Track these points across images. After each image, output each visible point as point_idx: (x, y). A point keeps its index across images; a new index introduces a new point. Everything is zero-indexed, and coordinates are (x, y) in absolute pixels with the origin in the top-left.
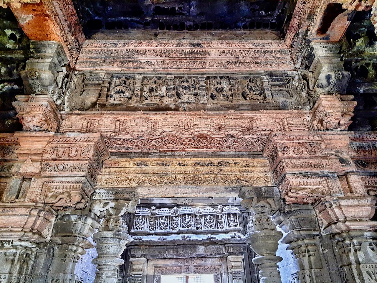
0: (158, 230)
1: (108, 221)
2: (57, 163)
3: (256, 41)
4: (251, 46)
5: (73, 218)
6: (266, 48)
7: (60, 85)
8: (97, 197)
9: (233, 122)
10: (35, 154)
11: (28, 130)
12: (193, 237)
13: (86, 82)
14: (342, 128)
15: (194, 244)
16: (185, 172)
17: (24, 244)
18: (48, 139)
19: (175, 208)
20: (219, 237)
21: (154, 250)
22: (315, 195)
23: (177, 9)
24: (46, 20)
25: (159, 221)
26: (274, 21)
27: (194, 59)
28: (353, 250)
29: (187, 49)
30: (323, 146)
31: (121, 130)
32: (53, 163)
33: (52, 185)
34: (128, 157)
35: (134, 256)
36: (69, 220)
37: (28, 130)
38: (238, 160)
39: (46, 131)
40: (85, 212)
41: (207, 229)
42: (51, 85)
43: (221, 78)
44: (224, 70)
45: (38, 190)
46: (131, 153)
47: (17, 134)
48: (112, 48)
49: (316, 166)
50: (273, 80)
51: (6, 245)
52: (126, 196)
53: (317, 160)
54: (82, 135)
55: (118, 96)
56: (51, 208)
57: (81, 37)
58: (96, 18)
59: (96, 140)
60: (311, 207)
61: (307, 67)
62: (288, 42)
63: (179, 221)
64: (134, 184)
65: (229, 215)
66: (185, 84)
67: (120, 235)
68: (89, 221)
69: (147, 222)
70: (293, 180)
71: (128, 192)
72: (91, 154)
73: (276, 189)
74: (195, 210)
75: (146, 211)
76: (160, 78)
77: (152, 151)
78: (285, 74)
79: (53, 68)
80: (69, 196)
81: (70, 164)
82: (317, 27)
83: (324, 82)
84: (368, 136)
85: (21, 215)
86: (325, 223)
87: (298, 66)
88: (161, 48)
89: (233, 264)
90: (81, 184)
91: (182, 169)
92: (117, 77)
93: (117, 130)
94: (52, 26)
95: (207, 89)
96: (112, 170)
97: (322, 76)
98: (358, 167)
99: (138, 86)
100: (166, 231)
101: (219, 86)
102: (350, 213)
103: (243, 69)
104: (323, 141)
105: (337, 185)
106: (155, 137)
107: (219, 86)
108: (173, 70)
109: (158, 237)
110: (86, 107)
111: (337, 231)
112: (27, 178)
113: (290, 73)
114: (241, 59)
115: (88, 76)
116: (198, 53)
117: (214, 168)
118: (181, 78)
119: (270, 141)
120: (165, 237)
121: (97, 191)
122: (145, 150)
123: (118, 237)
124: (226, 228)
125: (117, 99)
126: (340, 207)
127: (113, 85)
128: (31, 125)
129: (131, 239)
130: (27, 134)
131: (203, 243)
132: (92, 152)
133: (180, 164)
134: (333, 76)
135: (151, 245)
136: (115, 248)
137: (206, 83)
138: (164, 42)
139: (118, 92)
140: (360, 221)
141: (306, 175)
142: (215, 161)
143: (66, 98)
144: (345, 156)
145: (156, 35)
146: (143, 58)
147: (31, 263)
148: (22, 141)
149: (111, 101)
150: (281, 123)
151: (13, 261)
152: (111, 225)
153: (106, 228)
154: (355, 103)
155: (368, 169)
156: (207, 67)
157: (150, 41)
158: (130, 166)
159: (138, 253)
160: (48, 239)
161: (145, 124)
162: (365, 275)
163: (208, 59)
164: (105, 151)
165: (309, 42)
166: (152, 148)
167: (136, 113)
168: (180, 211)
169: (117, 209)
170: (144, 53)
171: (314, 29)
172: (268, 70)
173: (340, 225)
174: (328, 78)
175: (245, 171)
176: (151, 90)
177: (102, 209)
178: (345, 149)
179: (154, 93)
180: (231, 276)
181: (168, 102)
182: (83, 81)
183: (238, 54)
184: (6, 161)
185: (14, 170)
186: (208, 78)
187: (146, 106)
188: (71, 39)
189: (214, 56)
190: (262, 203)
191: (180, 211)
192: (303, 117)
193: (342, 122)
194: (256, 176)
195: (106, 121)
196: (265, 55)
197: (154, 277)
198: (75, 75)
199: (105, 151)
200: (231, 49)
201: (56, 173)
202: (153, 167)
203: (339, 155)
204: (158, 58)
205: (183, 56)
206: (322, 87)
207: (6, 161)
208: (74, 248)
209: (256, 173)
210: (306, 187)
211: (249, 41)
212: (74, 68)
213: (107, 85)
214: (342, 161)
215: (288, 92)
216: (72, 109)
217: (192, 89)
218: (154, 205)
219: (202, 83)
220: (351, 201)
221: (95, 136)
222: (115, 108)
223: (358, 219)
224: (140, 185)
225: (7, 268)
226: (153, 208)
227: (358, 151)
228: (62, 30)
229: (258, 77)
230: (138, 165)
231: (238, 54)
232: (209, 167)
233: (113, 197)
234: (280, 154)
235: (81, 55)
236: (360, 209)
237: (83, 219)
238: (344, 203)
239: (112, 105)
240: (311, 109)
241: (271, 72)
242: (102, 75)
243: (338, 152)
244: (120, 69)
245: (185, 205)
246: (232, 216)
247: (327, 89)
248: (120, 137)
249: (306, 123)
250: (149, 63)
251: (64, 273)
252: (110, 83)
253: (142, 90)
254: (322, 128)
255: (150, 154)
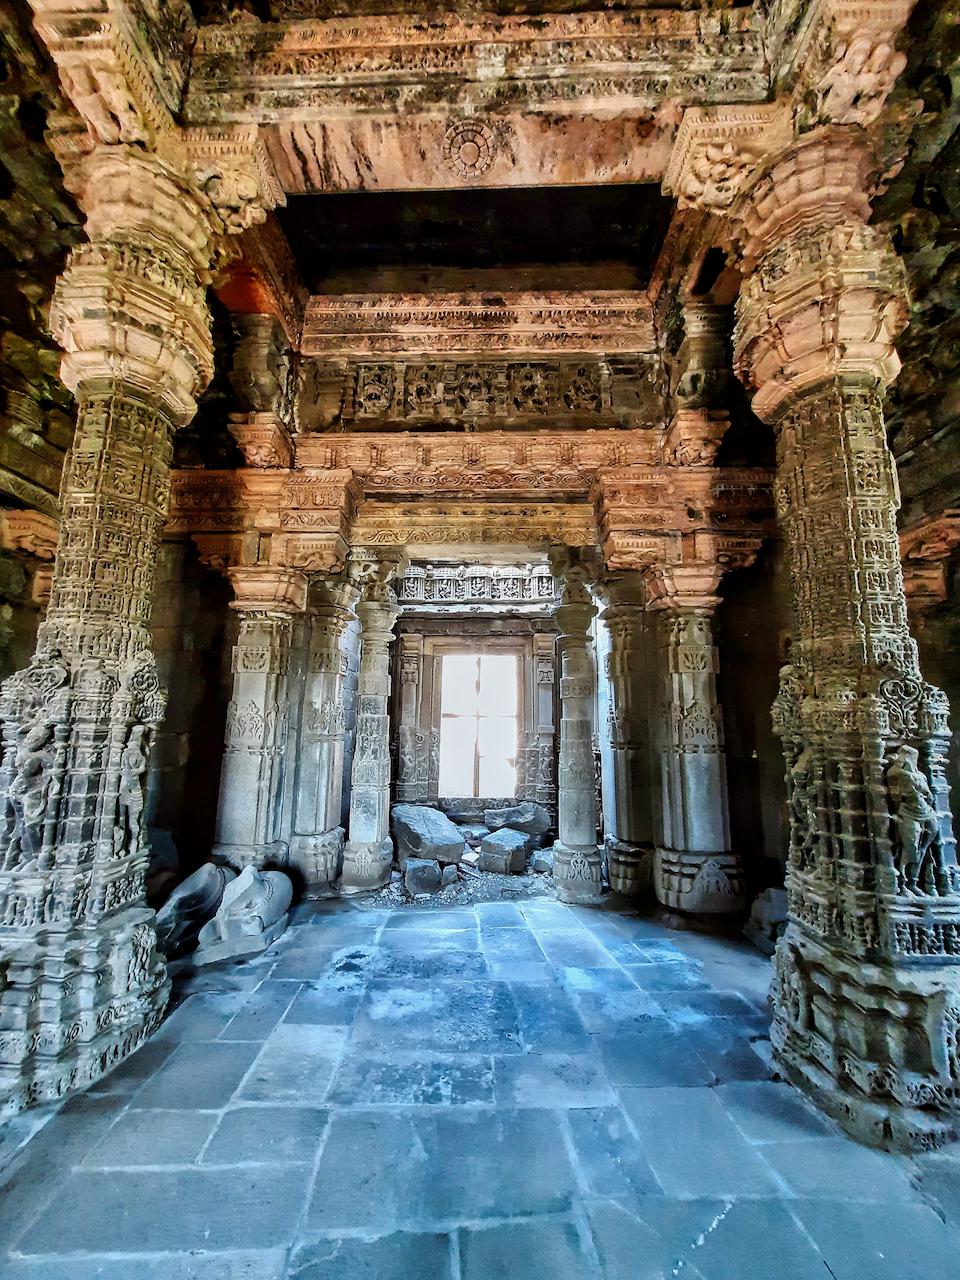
0: (437, 599)
1: (371, 588)
2: (300, 513)
3: (598, 293)
4: (588, 301)
5: (329, 584)
6: (615, 306)
7: (285, 391)
8: (353, 558)
9: (543, 449)
10: (269, 502)
11: (253, 466)
12: (487, 609)
13: (320, 380)
14: (704, 462)
15: (488, 619)
16: (472, 524)
17: (278, 615)
18: (282, 479)
19: (462, 567)
20: (524, 609)
21: (431, 625)
22: (645, 561)
23: (461, 223)
24: (252, 281)
25: (438, 586)
26: (636, 245)
27: (489, 331)
28: (676, 629)
29: (479, 309)
30: (671, 491)
31: (380, 463)
32: (294, 514)
33: (299, 544)
34: (389, 501)
35: (405, 631)
36: (324, 586)
37: (253, 466)
38: (549, 506)
39: (279, 467)
40: (342, 577)
41: (507, 598)
42: (273, 395)
43: (532, 365)
44: (538, 351)
45: (283, 550)
46: (395, 494)
47: (240, 472)
48: (354, 310)
49: (654, 520)
50: (617, 371)
51: (259, 616)
52: (393, 557)
53: (657, 512)
54: (327, 473)
55: (370, 404)
56: (303, 574)
57: (302, 292)
58: (323, 246)
59: (346, 480)
60: (639, 576)
61: (674, 351)
62: (653, 294)
63: (467, 586)
64: (402, 541)
65: (540, 578)
66: (474, 381)
67: (388, 606)
68: (348, 588)
69: (421, 586)
70: (618, 540)
71: (394, 552)
72: (342, 502)
73: (598, 549)
74: (491, 572)
75: (419, 571)
76: (434, 367)
77: (424, 491)
78: (638, 361)
79: (273, 365)
80: (321, 557)
81: (316, 515)
82: (692, 284)
83: (688, 387)
84: (741, 475)
85: (270, 581)
86: (654, 595)
87: (662, 344)
88: (433, 309)
89: (540, 644)
90: (334, 542)
91: (468, 519)
92: (365, 367)
93: (374, 464)
94: (261, 291)
95: (509, 388)
96: (371, 520)
97: (687, 376)
98: (713, 522)
99: (399, 385)
100: (448, 599)
101: (528, 384)
102: (683, 585)
103: (569, 349)
104: (671, 482)
105: (679, 545)
106: (428, 473)
107: (528, 384)
108: (455, 351)
109: (438, 608)
110: (325, 424)
111: (663, 607)
112: (265, 534)
113: (647, 357)
114: (569, 329)
115: (320, 365)
116: (498, 319)
117: (515, 519)
118: (467, 366)
119: (597, 481)
120: (447, 608)
121: (354, 550)
122: (414, 491)
123: (386, 608)
124: (535, 597)
125: (369, 410)
126: (671, 578)
127: (361, 383)
128: (257, 459)
129: (402, 609)
130: (253, 471)
131: (501, 617)
132: (343, 498)
133: (465, 513)
134: (703, 378)
135: (427, 618)
136: (384, 624)
137: (508, 377)
138: (439, 297)
139: (369, 397)
140: (694, 595)
141: (637, 533)
142: (516, 507)
143: (295, 409)
144: (699, 506)
145: (425, 279)
146: (405, 331)
147: (290, 636)
148: (249, 481)
149: (361, 414)
150: (617, 451)
151: (271, 633)
152: (376, 593)
153: (371, 598)
154: (729, 423)
155: (727, 526)
156: (510, 346)
157: (415, 295)
158: (394, 515)
159: (411, 627)
160: (304, 609)
161: (413, 454)
162: (681, 657)
163: (513, 330)
164: (363, 494)
165: (680, 307)
166: (425, 488)
167: (398, 434)
168: (470, 571)
169: (381, 574)
170: (407, 320)
171: (687, 287)
172: (611, 351)
173: (666, 600)
174: (695, 379)
175: (558, 523)
176: (420, 392)
177: (362, 574)
178: (700, 495)
179: (424, 399)
180: (536, 658)
181: (447, 413)
182: (315, 377)
183: (564, 320)
184: (233, 510)
185: (247, 523)
186: (511, 366)
187: (413, 421)
188: (289, 301)
189: (523, 328)
190: (576, 569)
191: (470, 571)
192: (650, 442)
193: (703, 454)
194: (573, 530)
195: (357, 449)
196: (609, 323)
197: (433, 658)
198: (302, 365)
199: (363, 494)
200: (554, 307)
201: (300, 528)
202: (425, 516)
203: (690, 504)
204: (430, 329)
205: (471, 325)
206: (682, 393)
207: (233, 510)
208: (335, 620)
209: (575, 526)
210: (635, 549)
211: (586, 293)
212: (299, 352)
213: (352, 384)
214: (691, 513)
215: (637, 394)
216: (306, 430)
217: (484, 390)
218: (430, 563)
219: (502, 378)
220: (689, 569)
221: (344, 474)
222: (367, 427)
223: (693, 593)
224: (409, 542)
225: (268, 641)
226: (429, 567)
227: (720, 498)
228: (276, 293)
229: (592, 365)
230: (404, 513)
231: (564, 320)
232: (507, 517)
233: (375, 558)
234: (606, 501)
235: (305, 328)
236: (698, 580)
237: (340, 586)
238: (678, 572)
239: (363, 420)
240: (666, 427)
241: (615, 355)
242: (343, 365)
243: (689, 500)
244: (370, 353)
245: (477, 563)
246: (545, 580)
247: (691, 398)
248: (379, 473)
249: (653, 452)
250: (415, 341)
251: (328, 647)
252: (356, 379)
253: (407, 392)
254: (675, 463)
255: (422, 496)
